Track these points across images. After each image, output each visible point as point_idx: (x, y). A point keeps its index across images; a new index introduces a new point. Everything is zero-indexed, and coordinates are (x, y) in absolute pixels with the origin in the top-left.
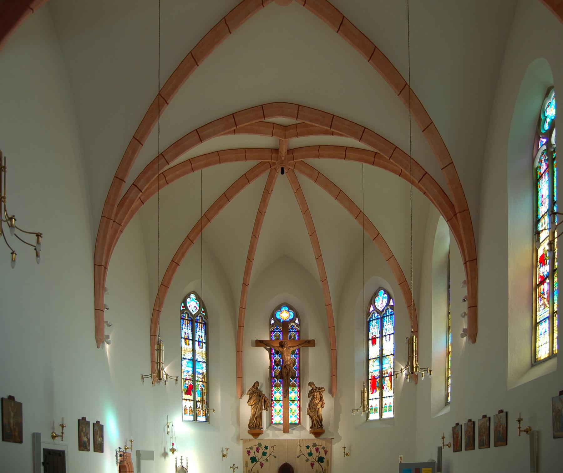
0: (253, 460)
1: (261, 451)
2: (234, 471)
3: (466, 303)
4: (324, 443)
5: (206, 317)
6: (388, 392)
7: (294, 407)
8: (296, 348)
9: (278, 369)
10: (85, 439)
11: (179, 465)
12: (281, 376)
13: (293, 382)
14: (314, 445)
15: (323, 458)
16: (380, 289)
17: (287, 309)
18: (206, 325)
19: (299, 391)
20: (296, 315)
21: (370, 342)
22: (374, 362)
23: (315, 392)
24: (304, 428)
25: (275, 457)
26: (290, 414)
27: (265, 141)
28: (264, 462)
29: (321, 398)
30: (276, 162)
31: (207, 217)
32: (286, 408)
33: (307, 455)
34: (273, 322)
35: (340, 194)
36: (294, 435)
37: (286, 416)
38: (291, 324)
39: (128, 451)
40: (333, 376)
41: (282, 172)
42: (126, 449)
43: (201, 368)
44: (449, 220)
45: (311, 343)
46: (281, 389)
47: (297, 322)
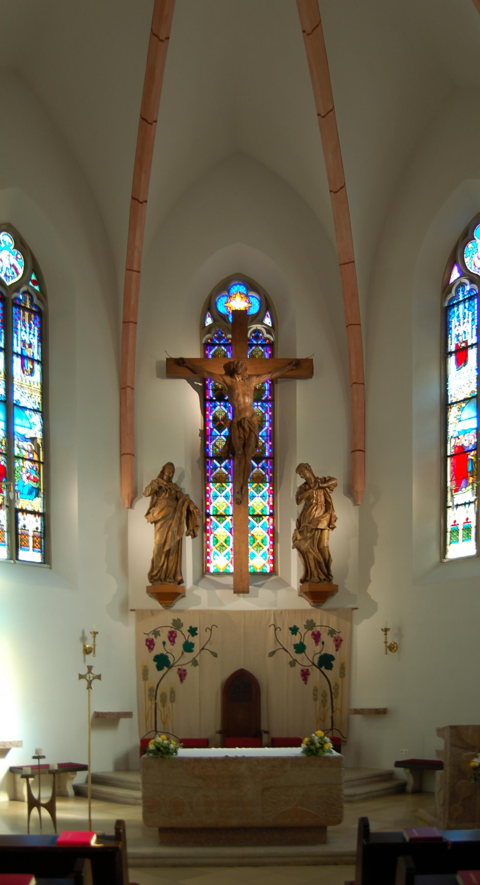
0: (162, 662)
1: (180, 640)
2: (89, 687)
4: (333, 621)
5: (43, 295)
7: (259, 531)
8: (266, 377)
9: (220, 439)
12: (228, 452)
13: (257, 468)
14: (310, 625)
15: (332, 658)
17: (243, 289)
18: (40, 315)
19: (273, 493)
20: (267, 305)
21: (452, 360)
22: (461, 409)
23: (313, 489)
24: (285, 584)
25: (215, 655)
26: (251, 550)
28: (189, 668)
29: (328, 506)
33: (292, 650)
34: (209, 321)
36: (261, 601)
38: (254, 327)
40: (357, 451)
45: (302, 368)
46: (229, 488)
47: (268, 321)
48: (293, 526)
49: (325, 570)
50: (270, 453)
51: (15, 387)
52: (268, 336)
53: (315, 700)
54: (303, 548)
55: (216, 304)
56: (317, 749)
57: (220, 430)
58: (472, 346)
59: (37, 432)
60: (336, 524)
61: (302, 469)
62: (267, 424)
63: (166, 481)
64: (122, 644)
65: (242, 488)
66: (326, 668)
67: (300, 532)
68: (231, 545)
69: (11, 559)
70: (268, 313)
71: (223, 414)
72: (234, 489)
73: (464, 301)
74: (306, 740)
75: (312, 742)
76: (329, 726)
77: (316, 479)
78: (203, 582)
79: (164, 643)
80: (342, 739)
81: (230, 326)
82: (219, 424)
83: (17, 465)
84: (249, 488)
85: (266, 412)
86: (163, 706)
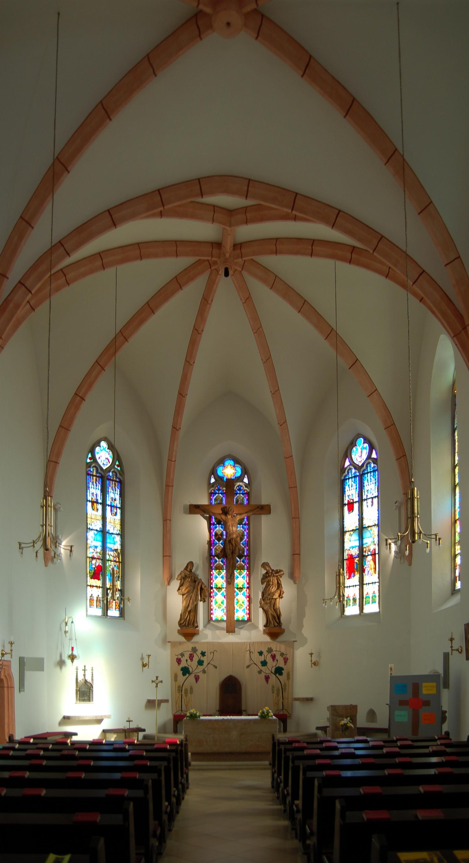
0: (185, 671)
1: (196, 659)
2: (157, 686)
5: (122, 472)
6: (371, 577)
7: (241, 598)
9: (220, 545)
11: (81, 678)
12: (223, 554)
13: (240, 562)
14: (270, 650)
15: (282, 669)
16: (358, 436)
17: (232, 463)
18: (121, 484)
19: (249, 575)
20: (245, 472)
21: (346, 508)
22: (351, 535)
23: (270, 576)
24: (256, 627)
25: (216, 667)
26: (236, 607)
27: (202, 230)
28: (201, 675)
29: (279, 585)
31: (123, 335)
32: (230, 598)
34: (213, 480)
35: (304, 306)
36: (242, 637)
37: (230, 610)
38: (238, 484)
40: (296, 554)
41: (227, 274)
45: (265, 509)
46: (224, 573)
47: (246, 480)
48: (260, 597)
49: (278, 621)
50: (247, 554)
51: (107, 523)
52: (246, 489)
53: (273, 692)
54: (265, 608)
55: (217, 471)
56: (265, 716)
57: (219, 541)
58: (356, 502)
59: (118, 546)
60: (283, 595)
61: (265, 565)
62: (245, 537)
63: (189, 572)
64: (164, 661)
65: (231, 576)
66: (279, 675)
67: (263, 600)
68: (225, 605)
69: (104, 615)
70: (246, 476)
71: (221, 532)
72: (227, 573)
73: (352, 478)
74: (261, 711)
75: (263, 712)
76: (281, 708)
77: (273, 570)
78: (209, 626)
79: (187, 661)
80: (288, 715)
81: (225, 484)
82: (219, 537)
83: (108, 564)
84: (235, 572)
85: (245, 530)
86: (186, 696)
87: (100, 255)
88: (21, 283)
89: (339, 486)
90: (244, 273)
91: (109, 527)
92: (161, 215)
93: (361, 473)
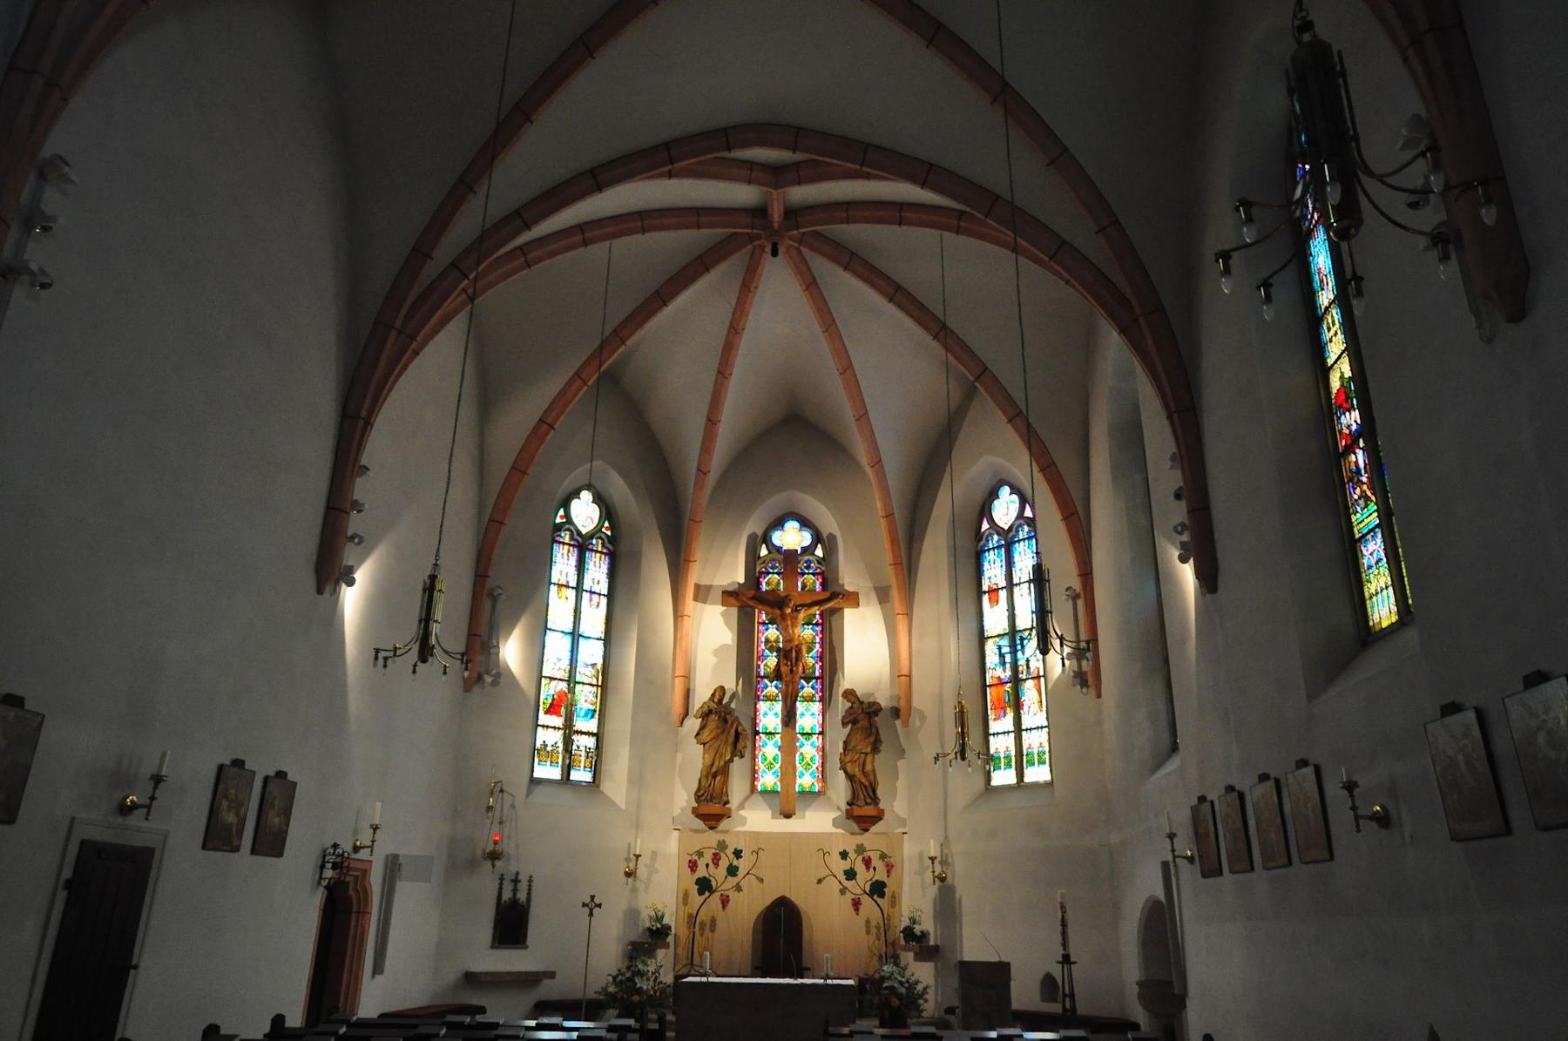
0: (704, 885)
1: (724, 863)
2: (591, 914)
3: (1183, 503)
6: (1034, 715)
7: (809, 750)
10: (231, 818)
11: (507, 895)
16: (1002, 483)
20: (818, 538)
27: (742, 194)
30: (751, 236)
32: (789, 749)
33: (842, 877)
37: (788, 772)
39: (363, 854)
41: (775, 253)
42: (356, 849)
43: (592, 652)
44: (1123, 331)
47: (819, 552)
87: (581, 228)
88: (453, 265)
89: (973, 561)
90: (804, 250)
91: (584, 629)
92: (670, 175)
93: (1009, 541)
